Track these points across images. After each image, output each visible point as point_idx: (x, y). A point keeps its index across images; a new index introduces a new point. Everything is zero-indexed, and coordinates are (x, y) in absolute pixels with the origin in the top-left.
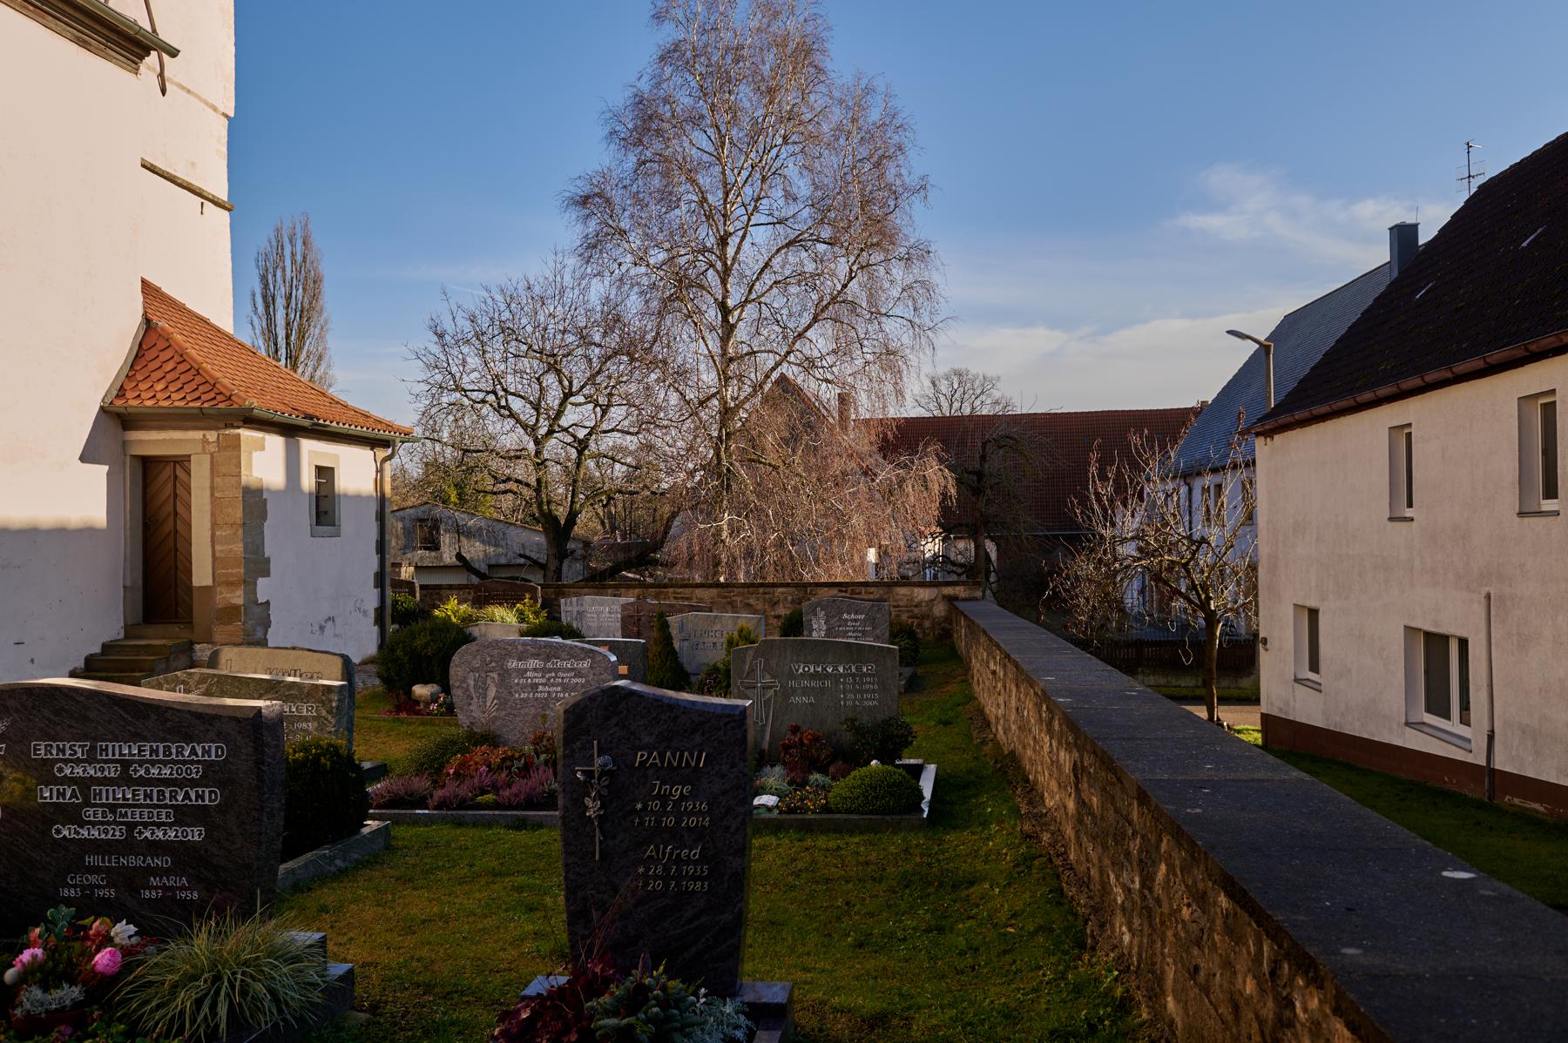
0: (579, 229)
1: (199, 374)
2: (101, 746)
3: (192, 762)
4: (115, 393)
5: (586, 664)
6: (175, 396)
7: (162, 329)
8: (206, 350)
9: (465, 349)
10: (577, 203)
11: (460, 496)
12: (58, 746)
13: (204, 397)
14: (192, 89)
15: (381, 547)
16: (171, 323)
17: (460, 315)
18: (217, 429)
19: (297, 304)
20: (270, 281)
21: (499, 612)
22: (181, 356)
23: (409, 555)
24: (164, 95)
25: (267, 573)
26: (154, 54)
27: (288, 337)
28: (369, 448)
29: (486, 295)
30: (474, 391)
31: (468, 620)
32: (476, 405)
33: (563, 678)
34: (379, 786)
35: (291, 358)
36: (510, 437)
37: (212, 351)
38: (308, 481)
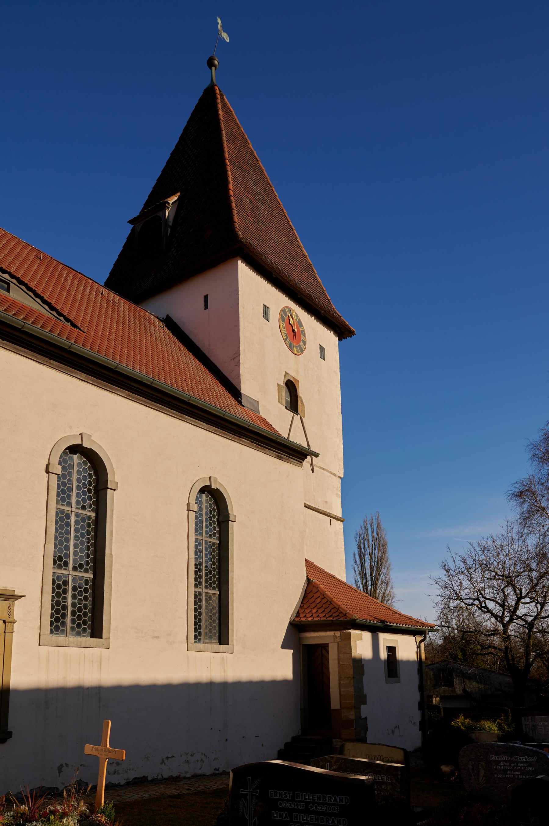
0: (519, 509)
1: (331, 603)
2: (297, 794)
3: (335, 805)
4: (295, 615)
5: (534, 759)
6: (321, 615)
7: (315, 583)
8: (334, 591)
9: (461, 577)
10: (518, 496)
11: (464, 655)
12: (279, 792)
13: (334, 615)
14: (325, 468)
15: (421, 688)
16: (318, 580)
17: (457, 559)
18: (340, 630)
19: (375, 558)
20: (362, 547)
21: (487, 724)
22: (323, 595)
23: (437, 689)
24: (313, 473)
25: (365, 703)
26: (309, 457)
27: (371, 574)
28: (412, 636)
29: (470, 547)
30: (467, 599)
31: (470, 728)
32: (468, 607)
33: (521, 767)
34: (424, 822)
35: (373, 585)
36: (489, 623)
37: (337, 592)
38: (383, 654)
